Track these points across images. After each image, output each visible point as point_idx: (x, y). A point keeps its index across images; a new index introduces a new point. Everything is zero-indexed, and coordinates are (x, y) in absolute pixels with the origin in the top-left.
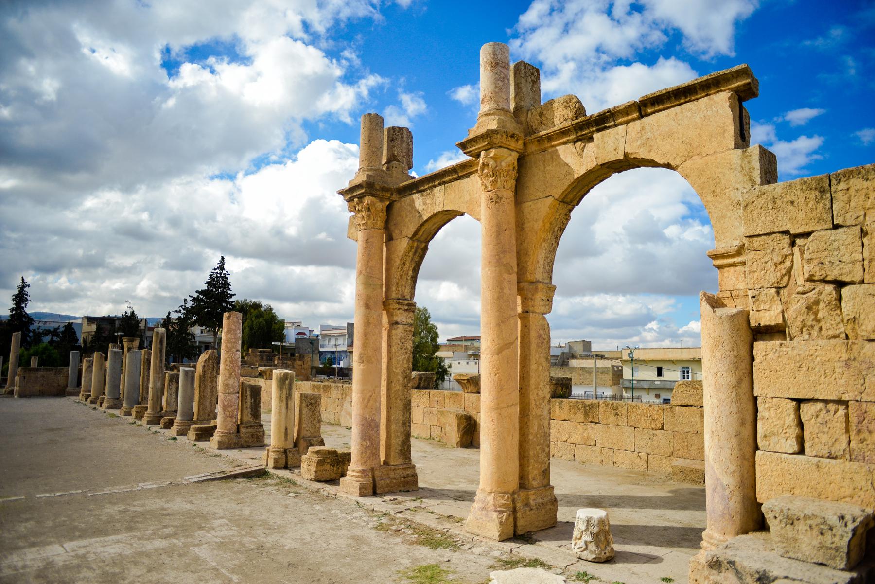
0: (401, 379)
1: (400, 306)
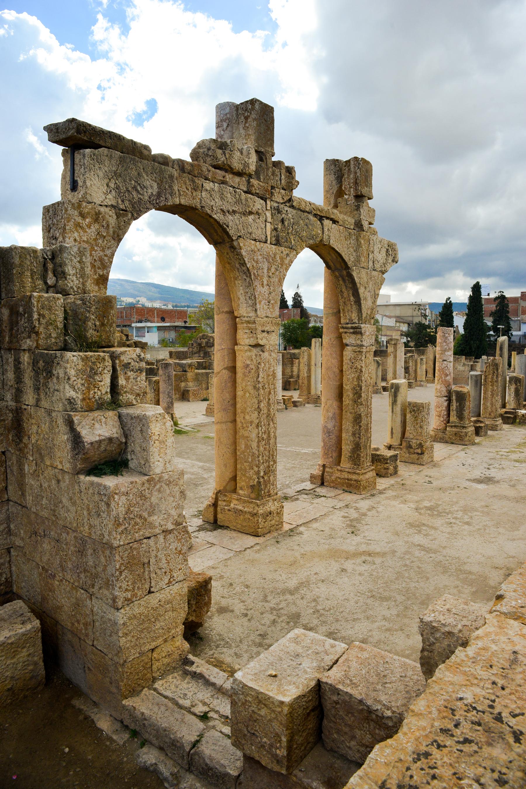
0: (351, 396)
1: (345, 330)
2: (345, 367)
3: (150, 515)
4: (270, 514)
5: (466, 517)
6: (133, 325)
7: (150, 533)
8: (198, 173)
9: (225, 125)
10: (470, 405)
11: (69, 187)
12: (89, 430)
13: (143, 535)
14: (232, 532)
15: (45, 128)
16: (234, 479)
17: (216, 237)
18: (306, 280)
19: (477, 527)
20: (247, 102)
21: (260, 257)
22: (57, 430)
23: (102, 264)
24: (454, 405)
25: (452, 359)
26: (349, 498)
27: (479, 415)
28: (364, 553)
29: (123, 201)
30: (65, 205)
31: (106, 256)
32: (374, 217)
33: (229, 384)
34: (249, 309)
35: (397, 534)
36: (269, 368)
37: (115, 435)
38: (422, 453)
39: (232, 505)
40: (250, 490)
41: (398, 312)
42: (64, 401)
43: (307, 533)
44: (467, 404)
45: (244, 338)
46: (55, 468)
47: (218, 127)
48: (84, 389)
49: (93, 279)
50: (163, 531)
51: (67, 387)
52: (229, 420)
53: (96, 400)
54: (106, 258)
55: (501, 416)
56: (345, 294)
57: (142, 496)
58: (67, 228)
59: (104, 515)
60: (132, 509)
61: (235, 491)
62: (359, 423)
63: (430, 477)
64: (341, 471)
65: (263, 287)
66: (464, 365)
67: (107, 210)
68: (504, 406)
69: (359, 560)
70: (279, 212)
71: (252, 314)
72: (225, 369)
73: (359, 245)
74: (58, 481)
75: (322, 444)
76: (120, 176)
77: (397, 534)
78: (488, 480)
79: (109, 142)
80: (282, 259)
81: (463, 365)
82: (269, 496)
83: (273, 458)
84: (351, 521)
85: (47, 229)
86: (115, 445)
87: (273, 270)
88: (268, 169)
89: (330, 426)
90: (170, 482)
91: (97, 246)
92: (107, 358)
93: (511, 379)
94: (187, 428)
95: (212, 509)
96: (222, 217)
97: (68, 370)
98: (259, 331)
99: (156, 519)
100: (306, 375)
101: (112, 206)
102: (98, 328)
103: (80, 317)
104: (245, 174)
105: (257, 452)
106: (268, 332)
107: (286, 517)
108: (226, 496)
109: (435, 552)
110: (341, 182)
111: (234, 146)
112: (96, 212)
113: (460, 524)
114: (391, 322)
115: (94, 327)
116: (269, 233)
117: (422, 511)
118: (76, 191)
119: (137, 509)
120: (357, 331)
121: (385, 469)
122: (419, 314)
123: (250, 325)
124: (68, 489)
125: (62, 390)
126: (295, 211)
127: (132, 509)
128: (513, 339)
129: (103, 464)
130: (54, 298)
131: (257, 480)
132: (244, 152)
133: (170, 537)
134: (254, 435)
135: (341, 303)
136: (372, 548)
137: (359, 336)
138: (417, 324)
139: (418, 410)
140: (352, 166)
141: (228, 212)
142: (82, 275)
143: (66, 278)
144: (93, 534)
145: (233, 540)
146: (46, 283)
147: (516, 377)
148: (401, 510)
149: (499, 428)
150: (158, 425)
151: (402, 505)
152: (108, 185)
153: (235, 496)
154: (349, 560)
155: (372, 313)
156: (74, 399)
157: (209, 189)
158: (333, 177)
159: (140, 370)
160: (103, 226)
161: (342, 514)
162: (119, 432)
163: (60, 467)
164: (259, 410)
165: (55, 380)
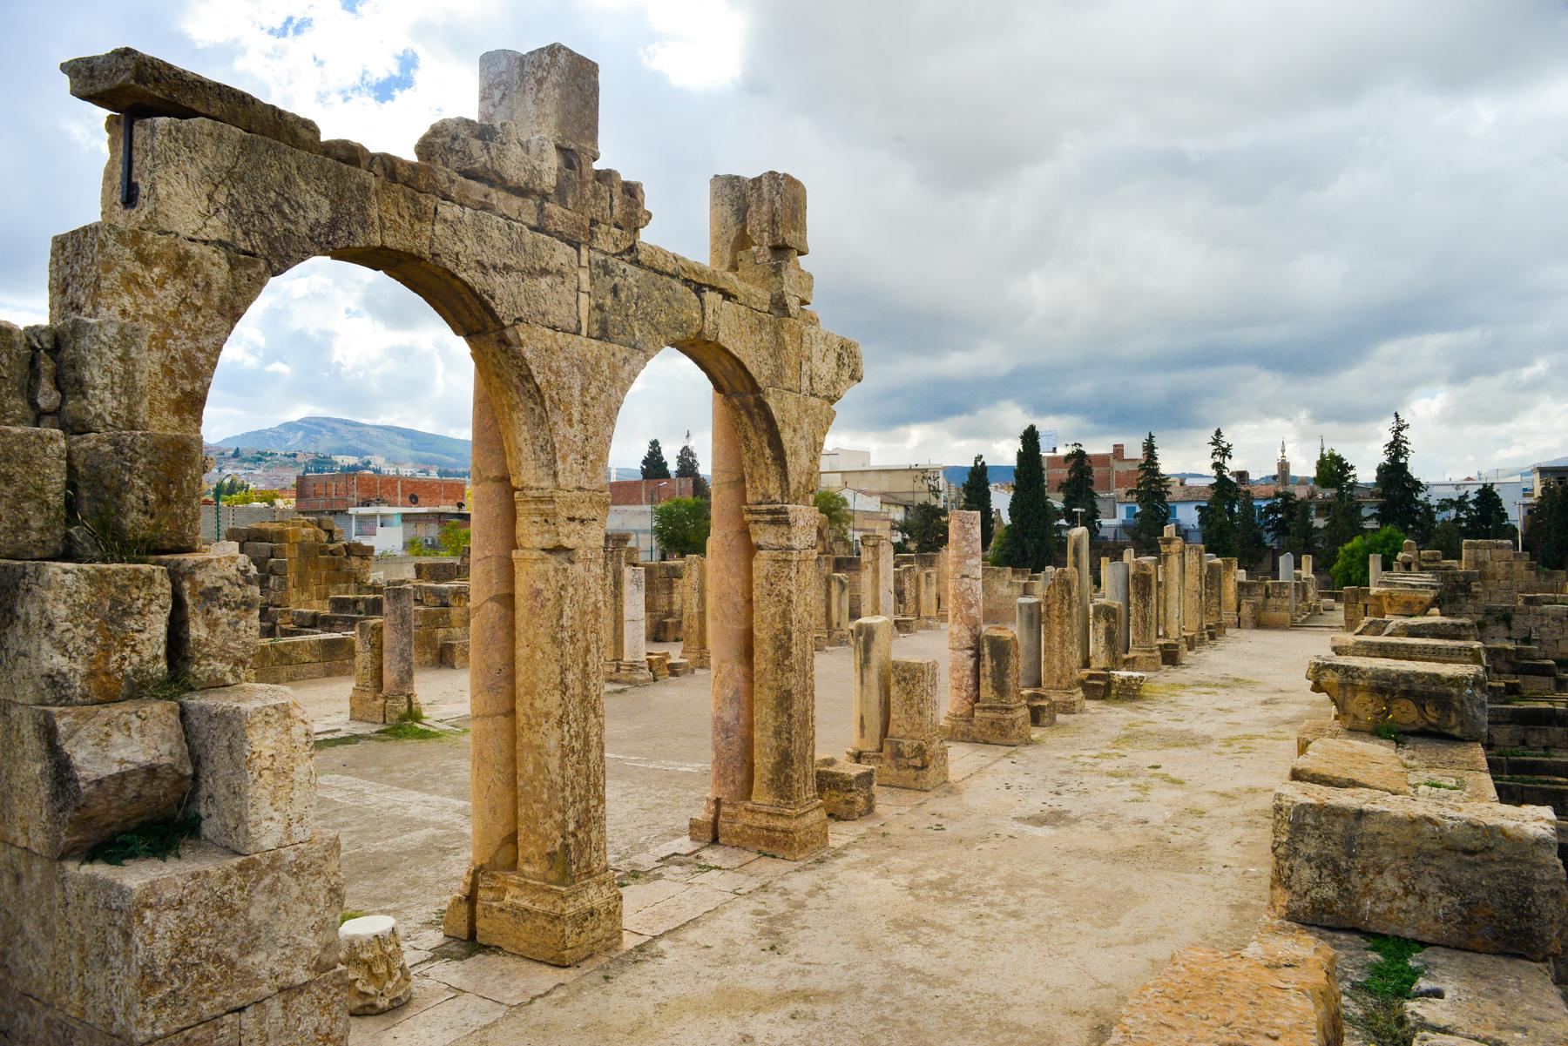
0: (770, 652)
1: (756, 517)
2: (756, 594)
3: (244, 951)
4: (592, 914)
5: (1012, 900)
6: (352, 511)
7: (243, 996)
8: (428, 185)
9: (497, 94)
10: (1020, 663)
11: (118, 197)
12: (93, 749)
13: (223, 1005)
14: (508, 959)
15: (64, 67)
16: (512, 839)
17: (468, 320)
18: (665, 408)
19: (1035, 922)
20: (542, 50)
21: (564, 364)
22: (20, 752)
23: (191, 367)
24: (988, 665)
25: (979, 573)
26: (769, 868)
27: (1038, 684)
28: (794, 995)
29: (246, 234)
30: (101, 235)
31: (200, 350)
32: (810, 289)
33: (500, 634)
34: (541, 473)
35: (866, 946)
36: (586, 598)
37: (166, 760)
38: (924, 767)
39: (508, 898)
40: (546, 863)
41: (885, 484)
42: (37, 679)
43: (673, 955)
44: (1013, 661)
45: (531, 534)
46: (12, 845)
47: (483, 99)
48: (92, 649)
49: (168, 399)
50: (281, 990)
51: (46, 646)
52: (500, 710)
53: (126, 677)
54: (200, 355)
55: (1081, 683)
56: (754, 444)
57: (223, 906)
58: (104, 284)
59: (117, 962)
60: (192, 941)
61: (513, 866)
62: (787, 709)
63: (941, 816)
64: (752, 811)
65: (571, 426)
66: (1011, 584)
67: (207, 250)
68: (1086, 664)
69: (781, 1013)
70: (607, 271)
71: (547, 483)
72: (491, 599)
73: (780, 344)
74: (18, 878)
75: (713, 756)
76: (242, 180)
77: (866, 946)
78: (1055, 818)
79: (217, 107)
80: (613, 368)
81: (1008, 584)
82: (589, 874)
83: (596, 790)
84: (770, 921)
85: (61, 287)
86: (165, 784)
87: (593, 390)
88: (584, 184)
89: (728, 715)
90: (301, 868)
91: (180, 327)
92: (158, 576)
93: (1097, 609)
94: (441, 726)
95: (464, 908)
96: (479, 277)
97: (48, 606)
98: (561, 519)
99: (262, 962)
100: (695, 610)
101: (220, 242)
102: (152, 507)
103: (107, 482)
104: (533, 191)
105: (559, 779)
106: (582, 521)
107: (629, 920)
108: (494, 877)
109: (947, 983)
110: (744, 219)
111: (509, 133)
112: (178, 254)
113: (1000, 917)
114: (872, 504)
115: (142, 507)
116: (584, 314)
117: (922, 893)
118: (134, 206)
119: (208, 941)
120: (779, 519)
121: (847, 802)
122: (926, 487)
123: (543, 507)
124: (40, 897)
125: (34, 653)
126: (641, 272)
127: (192, 941)
128: (1102, 533)
129: (132, 832)
130: (39, 437)
131: (560, 841)
132: (533, 149)
133: (302, 1002)
134: (552, 743)
135: (747, 463)
136: (811, 982)
137: (784, 529)
138: (920, 506)
139: (913, 677)
140: (765, 189)
141: (495, 268)
142: (128, 385)
143: (84, 395)
144: (90, 1012)
145: (506, 980)
146: (33, 404)
147: (1106, 607)
148: (877, 891)
149: (1077, 708)
150: (271, 733)
151: (881, 881)
152: (210, 198)
153: (514, 878)
154: (761, 1014)
155: (809, 481)
156: (64, 675)
157: (450, 218)
158: (727, 210)
159: (248, 604)
160: (196, 286)
161: (753, 905)
162: (177, 750)
163: (22, 842)
164: (564, 687)
165: (20, 630)
